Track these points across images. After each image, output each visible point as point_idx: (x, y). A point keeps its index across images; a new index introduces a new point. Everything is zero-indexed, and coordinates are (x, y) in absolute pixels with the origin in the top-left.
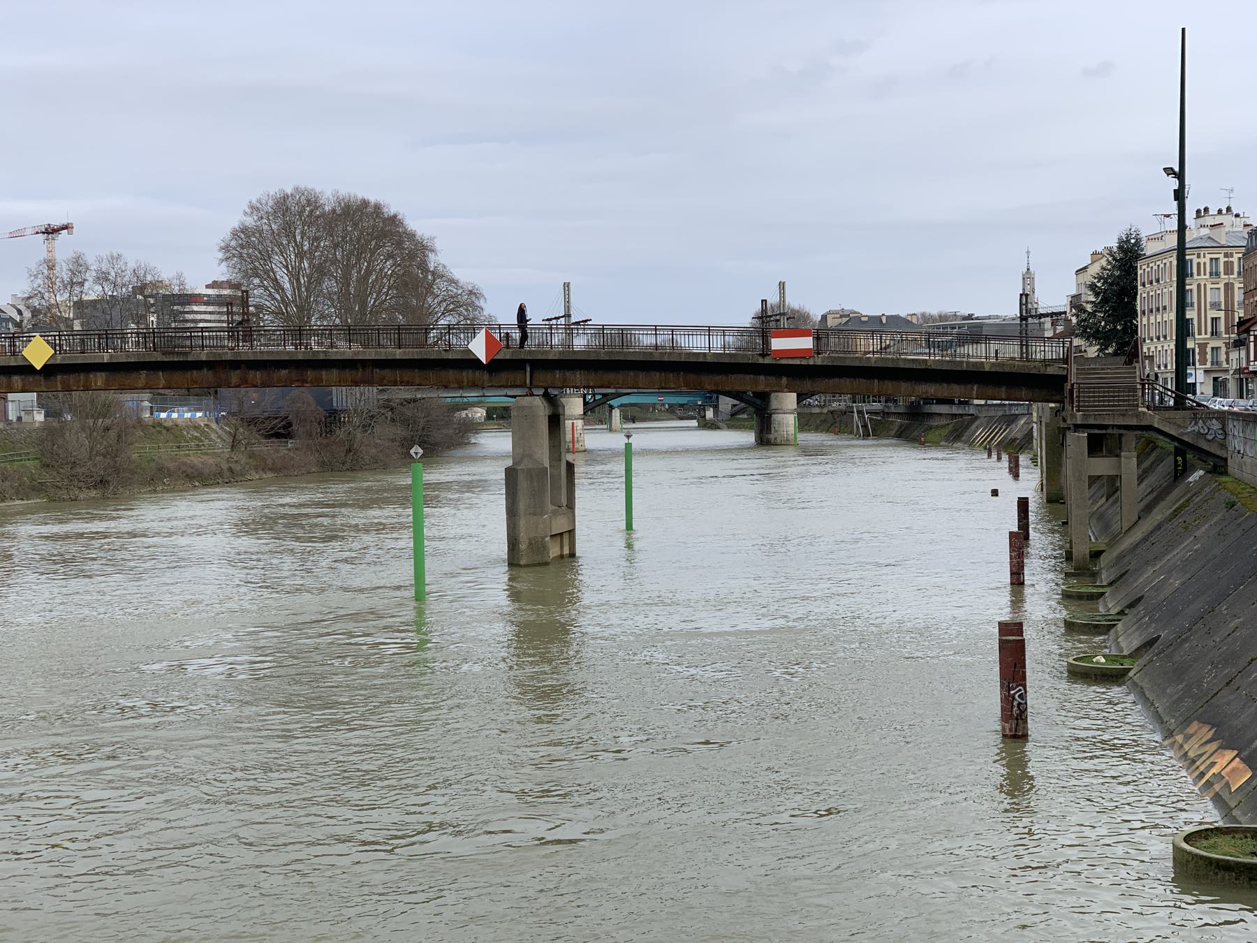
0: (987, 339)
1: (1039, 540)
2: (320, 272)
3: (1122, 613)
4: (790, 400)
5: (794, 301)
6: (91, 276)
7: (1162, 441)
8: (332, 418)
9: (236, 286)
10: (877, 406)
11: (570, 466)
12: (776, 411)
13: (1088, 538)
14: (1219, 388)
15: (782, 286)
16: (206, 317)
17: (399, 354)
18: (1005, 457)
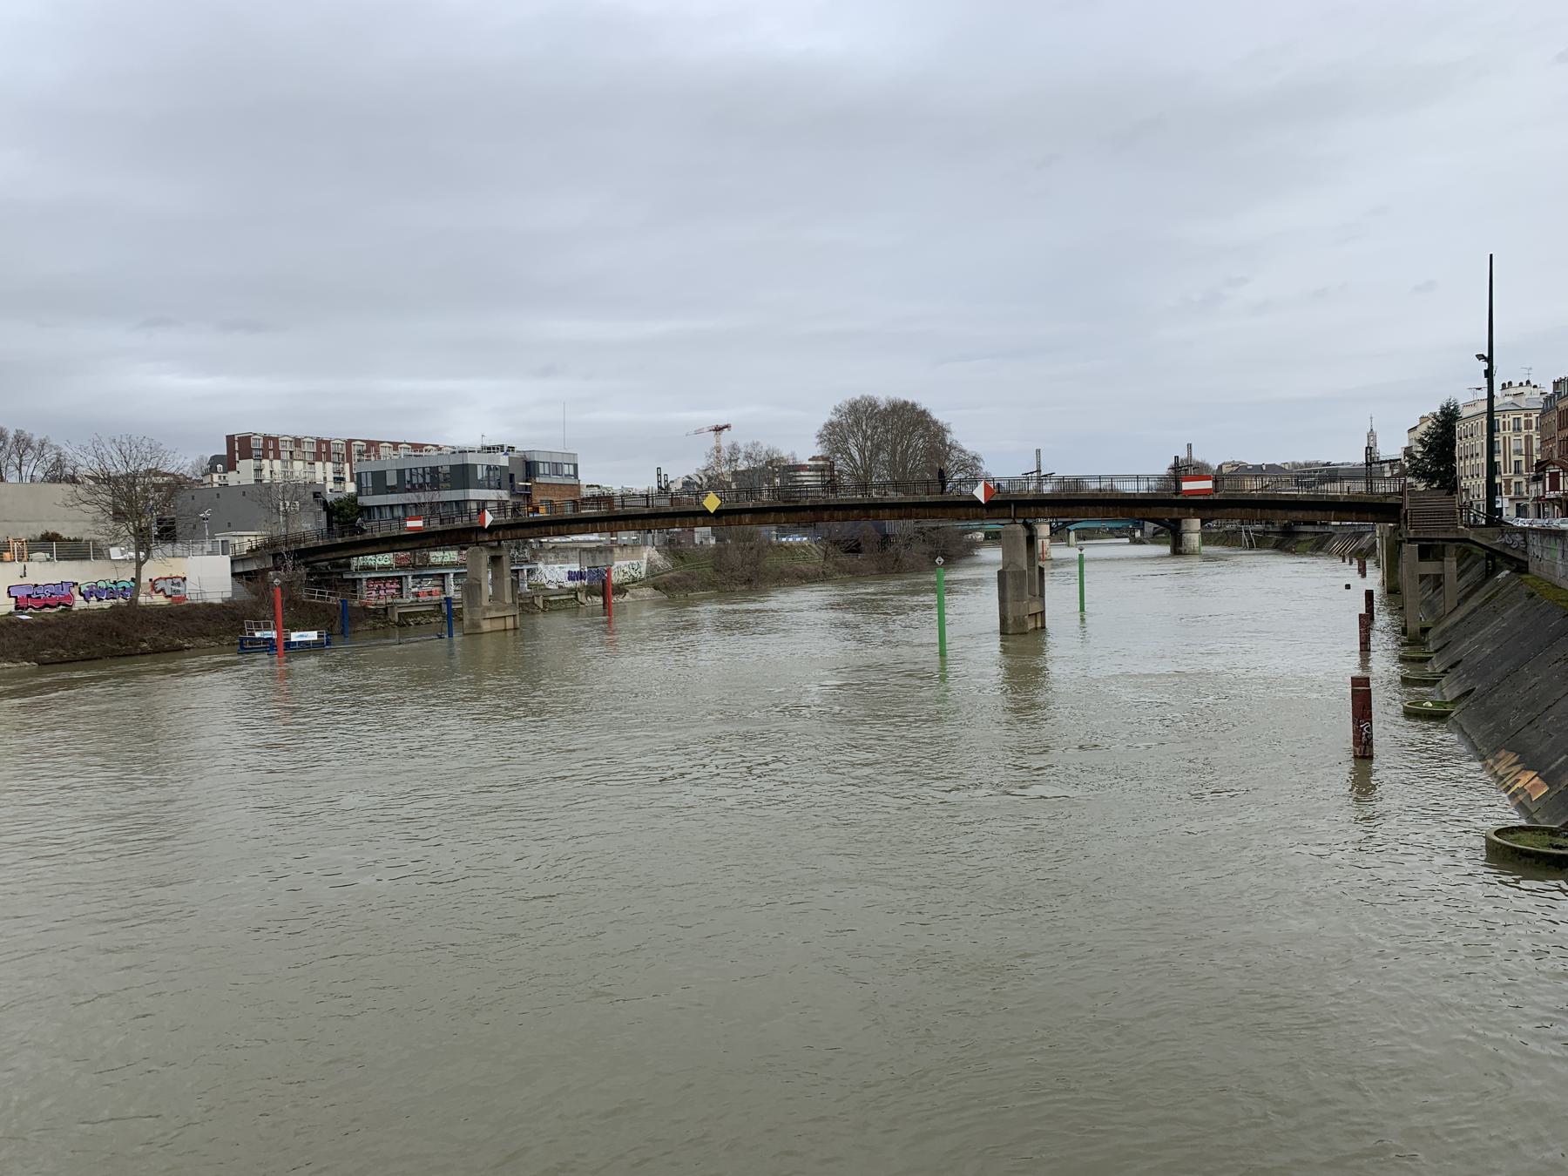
0: (1341, 479)
1: (1382, 619)
2: (878, 448)
3: (1445, 672)
4: (1196, 524)
5: (1198, 457)
6: (741, 456)
7: (1476, 549)
8: (886, 539)
9: (826, 459)
10: (1259, 527)
11: (1041, 570)
12: (1187, 531)
13: (1419, 618)
14: (1521, 511)
15: (1189, 446)
16: (808, 478)
17: (928, 499)
18: (1355, 562)
